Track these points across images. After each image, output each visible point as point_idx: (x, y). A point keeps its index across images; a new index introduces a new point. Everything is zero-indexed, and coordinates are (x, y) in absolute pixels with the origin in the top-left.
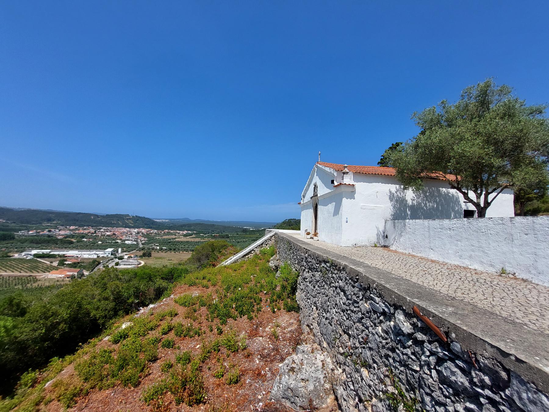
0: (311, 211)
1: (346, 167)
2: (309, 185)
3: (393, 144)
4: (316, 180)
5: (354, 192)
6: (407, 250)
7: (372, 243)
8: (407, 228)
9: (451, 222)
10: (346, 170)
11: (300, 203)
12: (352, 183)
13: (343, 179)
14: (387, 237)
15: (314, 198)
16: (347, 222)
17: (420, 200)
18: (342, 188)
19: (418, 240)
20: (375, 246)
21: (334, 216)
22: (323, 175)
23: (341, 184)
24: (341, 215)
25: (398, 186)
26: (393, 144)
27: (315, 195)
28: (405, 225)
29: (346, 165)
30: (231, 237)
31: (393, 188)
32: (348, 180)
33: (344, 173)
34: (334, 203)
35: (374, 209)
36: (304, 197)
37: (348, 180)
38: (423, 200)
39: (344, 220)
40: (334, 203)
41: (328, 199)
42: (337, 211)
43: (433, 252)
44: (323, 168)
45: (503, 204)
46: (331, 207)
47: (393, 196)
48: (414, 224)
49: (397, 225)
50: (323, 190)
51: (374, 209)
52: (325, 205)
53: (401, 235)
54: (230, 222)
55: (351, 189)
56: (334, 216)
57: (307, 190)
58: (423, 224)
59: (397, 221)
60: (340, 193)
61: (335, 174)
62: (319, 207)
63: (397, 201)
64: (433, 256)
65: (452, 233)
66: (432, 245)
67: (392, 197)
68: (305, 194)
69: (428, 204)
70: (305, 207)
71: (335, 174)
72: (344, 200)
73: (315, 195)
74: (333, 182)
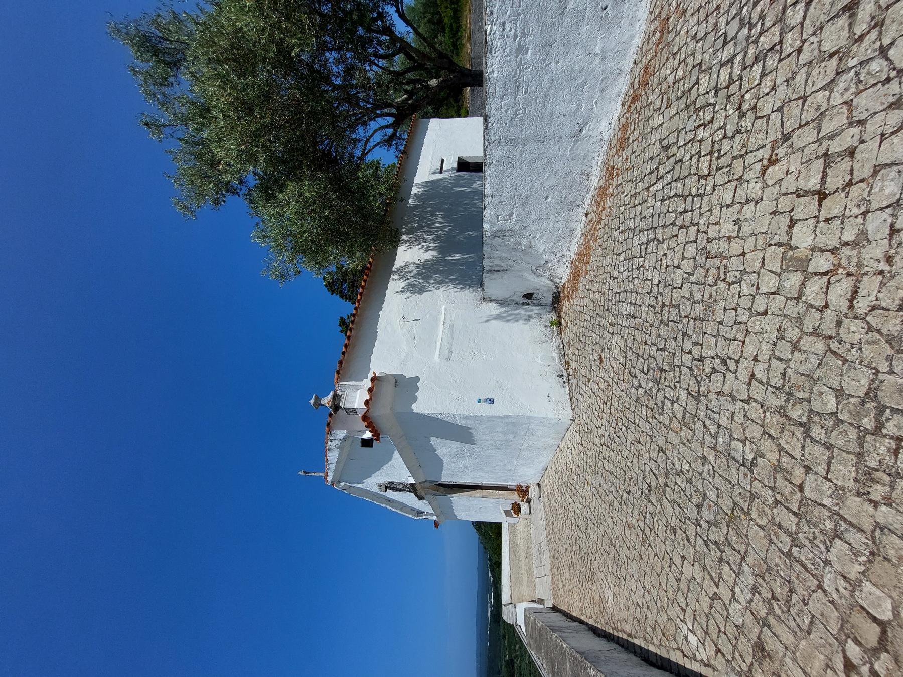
0: (458, 500)
1: (318, 399)
2: (390, 501)
3: (341, 332)
4: (372, 483)
5: (398, 380)
6: (573, 225)
7: (548, 332)
8: (509, 225)
9: (498, 43)
10: (326, 400)
11: (437, 524)
12: (367, 383)
13: (354, 411)
14: (529, 296)
15: (421, 492)
16: (491, 401)
17: (430, 238)
18: (381, 412)
19: (549, 184)
20: (559, 324)
21: (472, 442)
22: (352, 469)
23: (365, 418)
24: (467, 418)
25: (392, 277)
26: (341, 332)
27: (413, 489)
28: (499, 234)
29: (312, 401)
30: (510, 655)
31: (395, 285)
32: (356, 396)
33: (336, 408)
34: (433, 440)
35: (451, 327)
36: (419, 513)
37: (356, 396)
38: (429, 233)
39: (485, 410)
40: (433, 440)
41: (420, 456)
42: (460, 433)
43: (592, 124)
44: (332, 467)
45: (445, 141)
46: (444, 448)
47: (413, 286)
48: (496, 200)
49: (497, 262)
50: (397, 470)
51: (451, 327)
52: (439, 463)
53: (528, 250)
54: (479, 655)
55: (387, 390)
56: (472, 442)
57: (403, 506)
58: (498, 164)
59: (486, 263)
60: (392, 421)
61: (341, 434)
62: (446, 479)
63: (426, 279)
64: (607, 119)
65: (533, 39)
66: (569, 128)
67: (415, 289)
68: (413, 509)
69: (437, 225)
70: (447, 512)
71: (341, 434)
72: (418, 408)
73: (413, 489)
74: (366, 443)
